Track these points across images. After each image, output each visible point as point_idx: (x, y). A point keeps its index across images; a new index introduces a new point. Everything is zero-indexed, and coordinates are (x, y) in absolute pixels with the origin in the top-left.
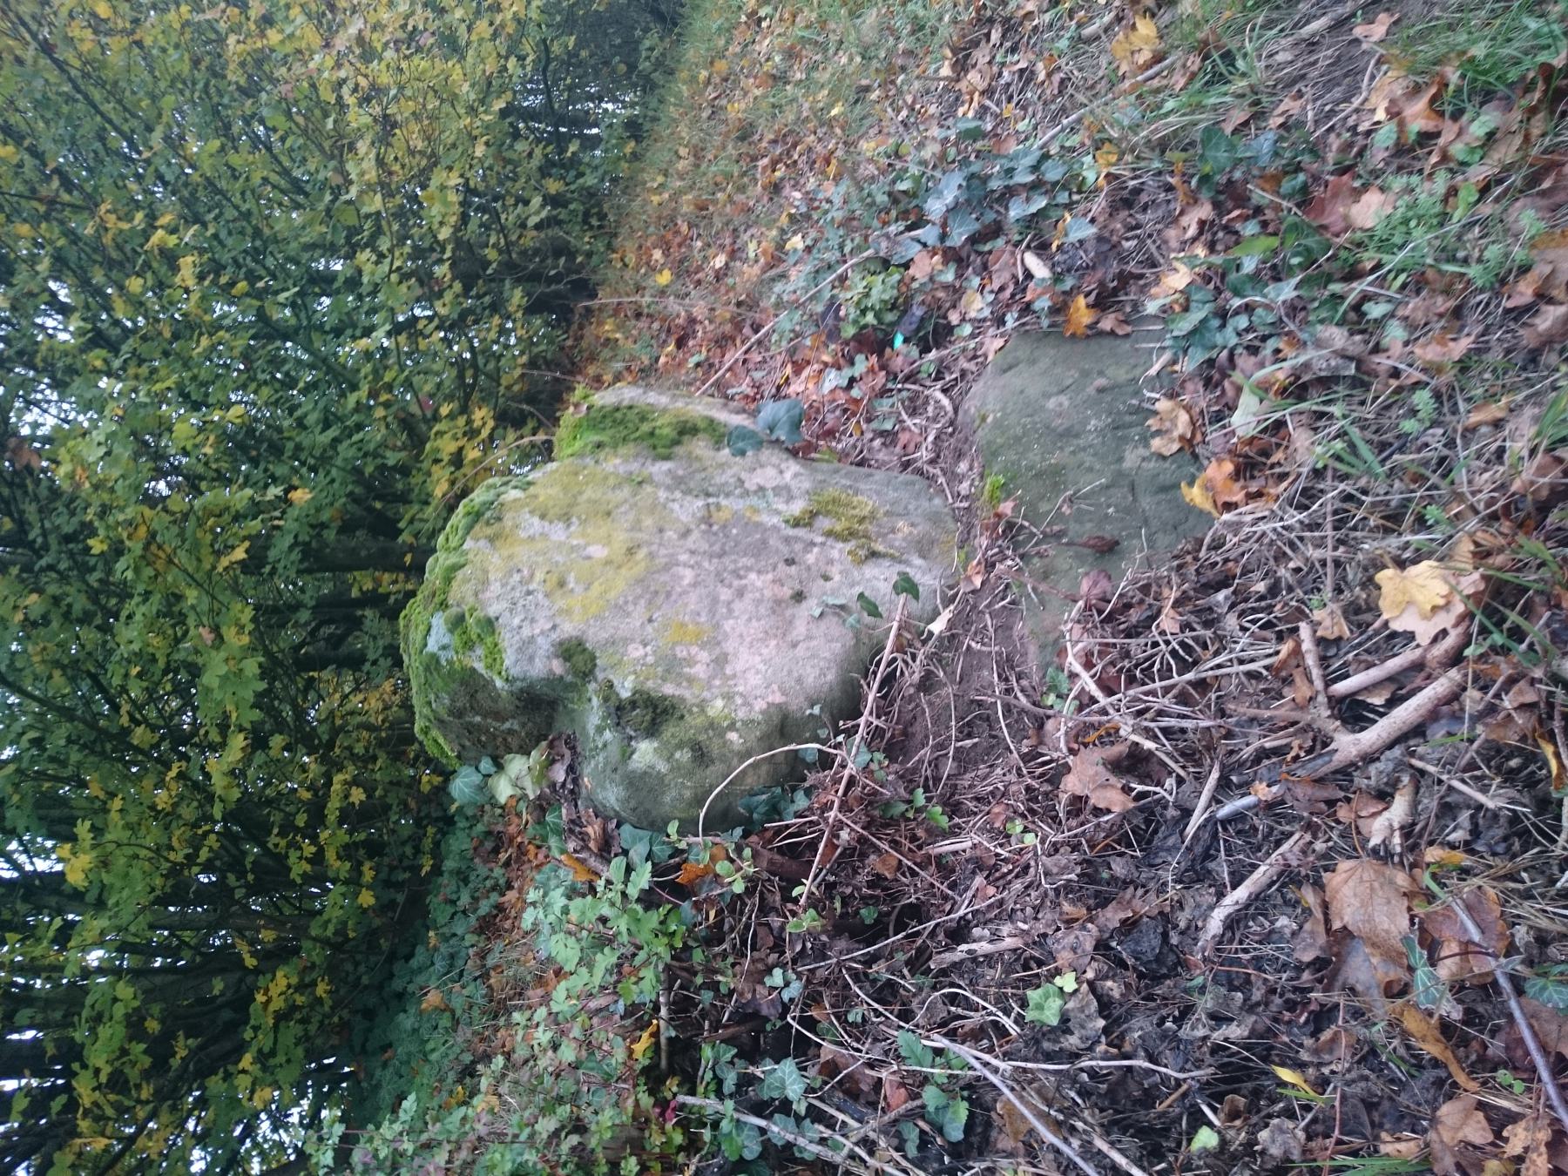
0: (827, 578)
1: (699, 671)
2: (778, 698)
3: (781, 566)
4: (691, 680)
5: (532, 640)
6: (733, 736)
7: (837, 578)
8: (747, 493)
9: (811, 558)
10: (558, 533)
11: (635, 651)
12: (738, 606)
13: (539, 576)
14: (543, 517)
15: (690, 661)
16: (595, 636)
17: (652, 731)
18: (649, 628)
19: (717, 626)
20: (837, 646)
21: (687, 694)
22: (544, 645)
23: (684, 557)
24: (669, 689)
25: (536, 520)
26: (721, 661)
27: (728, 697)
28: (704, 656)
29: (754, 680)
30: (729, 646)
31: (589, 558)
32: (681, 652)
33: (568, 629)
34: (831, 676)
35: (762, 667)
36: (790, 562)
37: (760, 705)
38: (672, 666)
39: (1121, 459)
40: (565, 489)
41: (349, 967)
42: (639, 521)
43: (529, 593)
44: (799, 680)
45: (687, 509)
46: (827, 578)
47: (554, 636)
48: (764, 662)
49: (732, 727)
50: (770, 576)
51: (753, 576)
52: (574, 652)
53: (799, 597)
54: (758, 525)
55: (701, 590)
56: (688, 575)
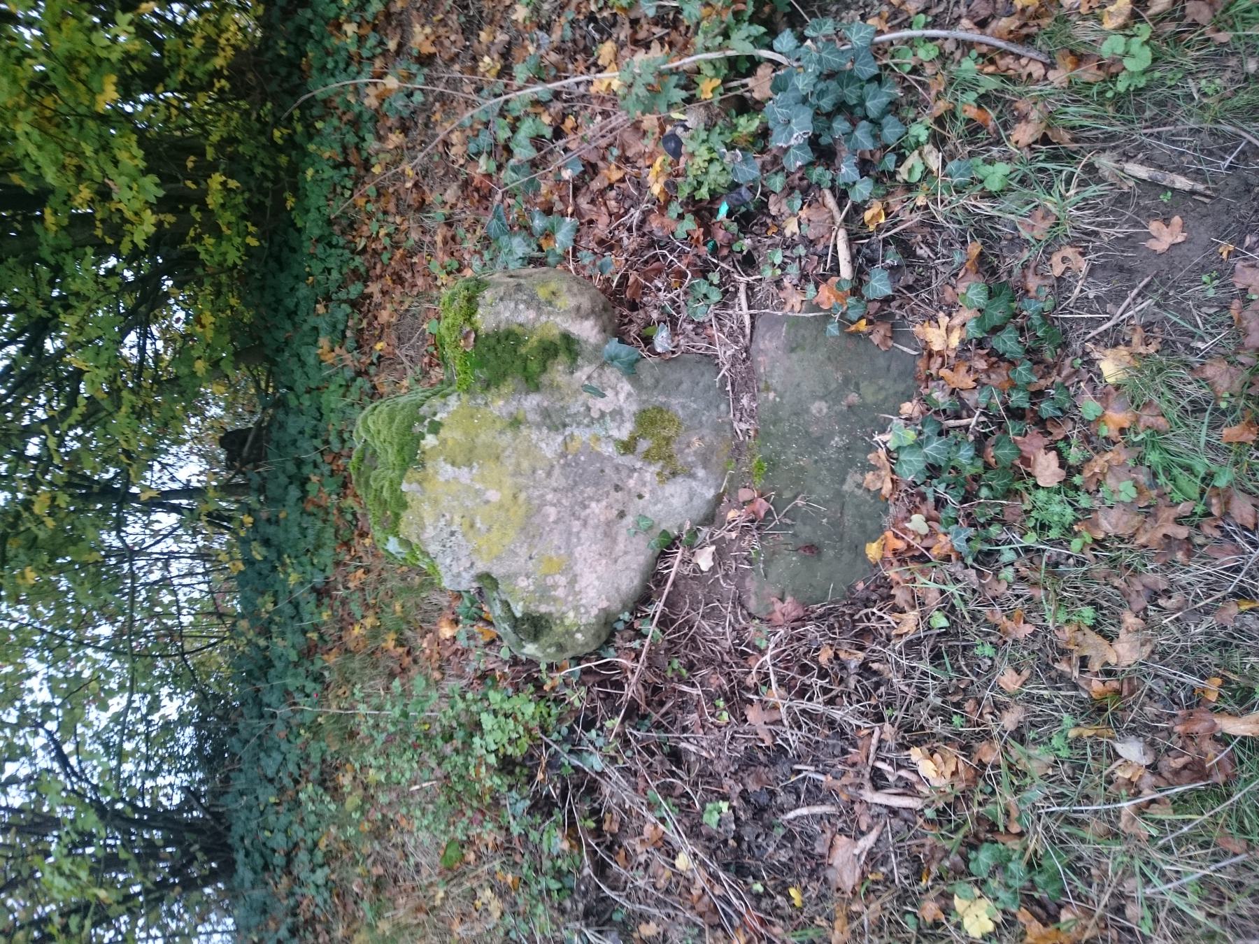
0: (640, 497)
1: (560, 593)
2: (604, 604)
3: (613, 493)
4: (555, 599)
5: (459, 575)
6: (579, 636)
7: (647, 496)
8: (592, 421)
9: (631, 483)
10: (464, 474)
11: (523, 583)
12: (583, 535)
13: (457, 519)
14: (453, 464)
15: (555, 587)
16: (497, 571)
17: (535, 638)
18: (530, 564)
19: (571, 555)
20: (641, 559)
21: (553, 609)
22: (467, 576)
23: (549, 497)
24: (543, 609)
25: (449, 467)
26: (573, 581)
27: (576, 608)
28: (562, 580)
29: (592, 593)
30: (577, 569)
31: (487, 502)
32: (550, 581)
33: (481, 567)
34: (636, 582)
35: (596, 583)
36: (617, 488)
37: (594, 611)
38: (544, 592)
39: (843, 481)
40: (466, 433)
41: (167, 598)
42: (518, 464)
43: (453, 533)
44: (618, 590)
45: (549, 446)
46: (640, 497)
47: (473, 572)
48: (598, 578)
49: (578, 631)
50: (604, 503)
51: (593, 505)
52: (487, 580)
53: (622, 515)
54: (599, 454)
55: (561, 527)
56: (552, 512)
